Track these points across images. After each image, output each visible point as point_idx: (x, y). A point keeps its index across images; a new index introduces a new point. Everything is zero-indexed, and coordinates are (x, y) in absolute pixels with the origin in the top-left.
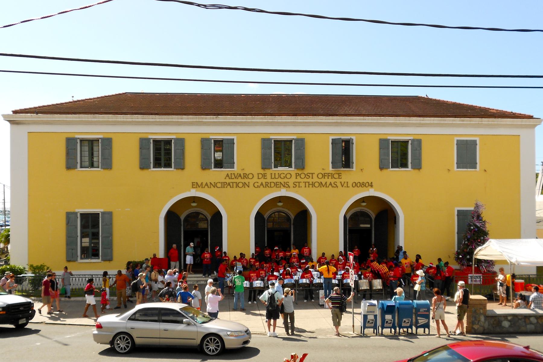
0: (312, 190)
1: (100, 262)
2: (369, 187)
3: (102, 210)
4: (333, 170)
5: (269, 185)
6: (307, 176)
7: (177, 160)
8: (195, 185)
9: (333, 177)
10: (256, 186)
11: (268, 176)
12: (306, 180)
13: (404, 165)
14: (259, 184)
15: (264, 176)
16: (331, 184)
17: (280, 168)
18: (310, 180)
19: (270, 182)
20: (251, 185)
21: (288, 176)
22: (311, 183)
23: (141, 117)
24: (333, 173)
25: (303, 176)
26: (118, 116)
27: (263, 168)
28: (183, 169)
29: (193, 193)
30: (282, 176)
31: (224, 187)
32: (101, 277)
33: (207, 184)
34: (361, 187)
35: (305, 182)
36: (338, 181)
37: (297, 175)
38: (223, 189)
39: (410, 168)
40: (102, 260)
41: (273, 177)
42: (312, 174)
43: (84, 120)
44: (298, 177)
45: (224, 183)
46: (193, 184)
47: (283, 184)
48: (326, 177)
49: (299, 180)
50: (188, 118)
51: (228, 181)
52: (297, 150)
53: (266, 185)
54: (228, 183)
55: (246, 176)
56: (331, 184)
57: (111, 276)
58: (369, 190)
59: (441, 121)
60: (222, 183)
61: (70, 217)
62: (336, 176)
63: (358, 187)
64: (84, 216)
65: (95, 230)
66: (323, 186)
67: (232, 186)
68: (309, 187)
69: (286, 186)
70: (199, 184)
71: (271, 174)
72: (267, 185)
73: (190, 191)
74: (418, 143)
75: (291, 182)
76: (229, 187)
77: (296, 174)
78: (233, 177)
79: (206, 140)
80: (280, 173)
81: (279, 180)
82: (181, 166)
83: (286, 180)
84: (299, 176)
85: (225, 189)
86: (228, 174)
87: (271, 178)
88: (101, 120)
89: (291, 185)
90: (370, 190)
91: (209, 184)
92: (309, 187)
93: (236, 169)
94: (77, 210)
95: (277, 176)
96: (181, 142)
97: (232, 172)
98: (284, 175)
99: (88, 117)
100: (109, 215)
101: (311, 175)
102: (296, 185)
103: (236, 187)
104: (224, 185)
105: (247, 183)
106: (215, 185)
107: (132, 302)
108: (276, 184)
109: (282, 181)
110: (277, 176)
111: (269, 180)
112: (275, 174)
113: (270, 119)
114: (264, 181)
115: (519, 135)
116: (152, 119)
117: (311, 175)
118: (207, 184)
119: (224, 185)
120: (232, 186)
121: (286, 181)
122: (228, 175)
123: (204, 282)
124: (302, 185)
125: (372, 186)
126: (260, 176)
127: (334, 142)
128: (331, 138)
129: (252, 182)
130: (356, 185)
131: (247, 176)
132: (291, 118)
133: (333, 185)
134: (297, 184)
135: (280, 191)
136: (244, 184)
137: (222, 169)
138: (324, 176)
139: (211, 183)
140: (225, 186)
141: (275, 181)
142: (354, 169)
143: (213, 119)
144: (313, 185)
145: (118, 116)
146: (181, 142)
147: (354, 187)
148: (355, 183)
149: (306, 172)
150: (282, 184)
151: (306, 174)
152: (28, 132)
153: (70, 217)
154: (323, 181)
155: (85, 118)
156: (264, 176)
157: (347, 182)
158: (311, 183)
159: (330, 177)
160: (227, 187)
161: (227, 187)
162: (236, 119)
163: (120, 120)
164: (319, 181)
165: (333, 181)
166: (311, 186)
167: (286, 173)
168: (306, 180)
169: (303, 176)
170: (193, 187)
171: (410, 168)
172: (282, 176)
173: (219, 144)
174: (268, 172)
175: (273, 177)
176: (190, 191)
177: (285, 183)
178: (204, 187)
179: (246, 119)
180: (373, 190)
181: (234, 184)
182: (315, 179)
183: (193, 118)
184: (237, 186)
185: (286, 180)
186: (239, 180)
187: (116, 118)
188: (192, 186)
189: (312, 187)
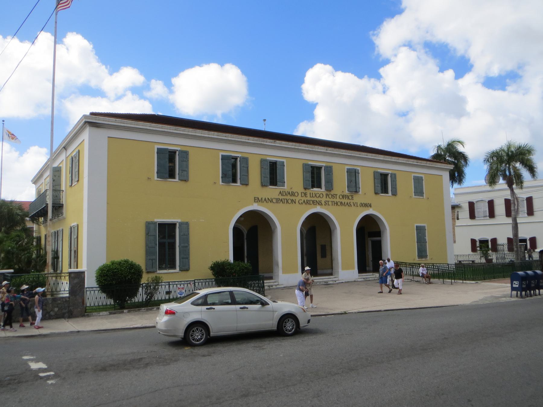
0: (336, 208)
1: (178, 272)
2: (370, 207)
3: (179, 221)
4: (223, 184)
5: (309, 202)
6: (334, 196)
7: (243, 176)
8: (257, 200)
9: (348, 198)
10: (300, 203)
11: (308, 195)
12: (332, 200)
13: (234, 181)
14: (302, 201)
15: (305, 194)
16: (347, 204)
17: (315, 189)
18: (335, 200)
19: (310, 200)
20: (297, 202)
21: (321, 196)
22: (335, 202)
23: (217, 134)
24: (349, 195)
25: (330, 196)
26: (197, 131)
27: (305, 189)
28: (247, 185)
29: (256, 207)
30: (318, 195)
31: (278, 203)
32: (96, 290)
33: (265, 199)
34: (365, 207)
35: (332, 202)
36: (352, 201)
37: (327, 195)
38: (277, 204)
39: (238, 184)
40: (180, 270)
41: (311, 196)
42: (336, 195)
43: (166, 130)
44: (327, 197)
45: (278, 199)
46: (255, 198)
47: (318, 202)
48: (345, 198)
49: (328, 199)
50: (218, 135)
51: (281, 197)
52: (327, 175)
53: (307, 202)
54: (281, 199)
55: (293, 194)
56: (347, 204)
57: (87, 289)
58: (369, 210)
59: (407, 161)
60: (276, 199)
61: (149, 225)
62: (350, 197)
63: (290, 203)
64: (162, 226)
65: (171, 241)
66: (260, 201)
67: (283, 202)
68: (334, 205)
69: (320, 203)
70: (260, 199)
71: (310, 193)
72: (307, 203)
73: (252, 205)
74: (185, 155)
75: (323, 200)
76: (281, 202)
77: (326, 194)
78: (284, 194)
79: (265, 161)
80: (316, 193)
81: (315, 199)
82: (245, 183)
83: (319, 199)
84: (328, 196)
85: (279, 204)
86: (280, 192)
87: (302, 196)
88: (290, 146)
89: (323, 203)
90: (317, 207)
91: (267, 199)
92: (334, 205)
93: (286, 188)
94: (156, 220)
95: (314, 195)
96: (245, 160)
97: (284, 190)
98: (319, 195)
99: (170, 128)
100: (185, 226)
101: (335, 196)
102: (326, 203)
103: (287, 203)
104: (278, 201)
105: (294, 200)
106: (271, 201)
107: (302, 302)
108: (313, 202)
109: (318, 199)
110: (314, 195)
111: (309, 198)
112: (313, 193)
113: (311, 148)
114: (305, 199)
115: (442, 175)
116: (225, 137)
117: (335, 196)
118: (265, 199)
119: (278, 201)
120: (283, 202)
121: (320, 200)
122: (280, 193)
123: (332, 282)
124: (330, 203)
125: (371, 206)
126: (303, 195)
127: (224, 158)
128: (157, 146)
129: (297, 199)
130: (362, 205)
131: (294, 194)
132: (150, 125)
133: (349, 204)
134: (327, 202)
135: (316, 207)
136: (292, 201)
137: (276, 187)
138: (343, 197)
139: (268, 199)
140: (279, 202)
141: (313, 199)
142: (360, 193)
143: (272, 143)
144: (337, 204)
145: (197, 131)
146: (245, 160)
147: (290, 203)
148: (361, 203)
149: (333, 192)
150: (269, 200)
151: (332, 194)
152: (108, 137)
153: (149, 225)
154: (343, 201)
155: (167, 129)
156: (306, 195)
157: (357, 203)
158: (335, 202)
159: (347, 198)
160: (280, 203)
161: (280, 203)
162: (109, 121)
163: (198, 135)
164: (341, 201)
165: (349, 201)
166: (335, 204)
167: (320, 193)
168: (332, 200)
169: (330, 196)
170: (255, 201)
171: (238, 184)
172: (318, 195)
173: (172, 155)
174: (308, 192)
175: (311, 196)
176: (252, 205)
177: (327, 204)
178: (263, 202)
179: (295, 146)
180: (372, 209)
181: (285, 200)
182: (338, 200)
183: (257, 140)
184: (287, 202)
185: (319, 199)
186: (288, 197)
187: (195, 133)
188: (254, 201)
189: (337, 205)
